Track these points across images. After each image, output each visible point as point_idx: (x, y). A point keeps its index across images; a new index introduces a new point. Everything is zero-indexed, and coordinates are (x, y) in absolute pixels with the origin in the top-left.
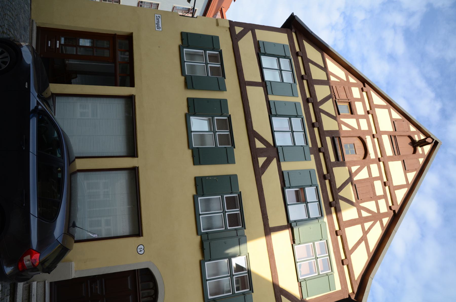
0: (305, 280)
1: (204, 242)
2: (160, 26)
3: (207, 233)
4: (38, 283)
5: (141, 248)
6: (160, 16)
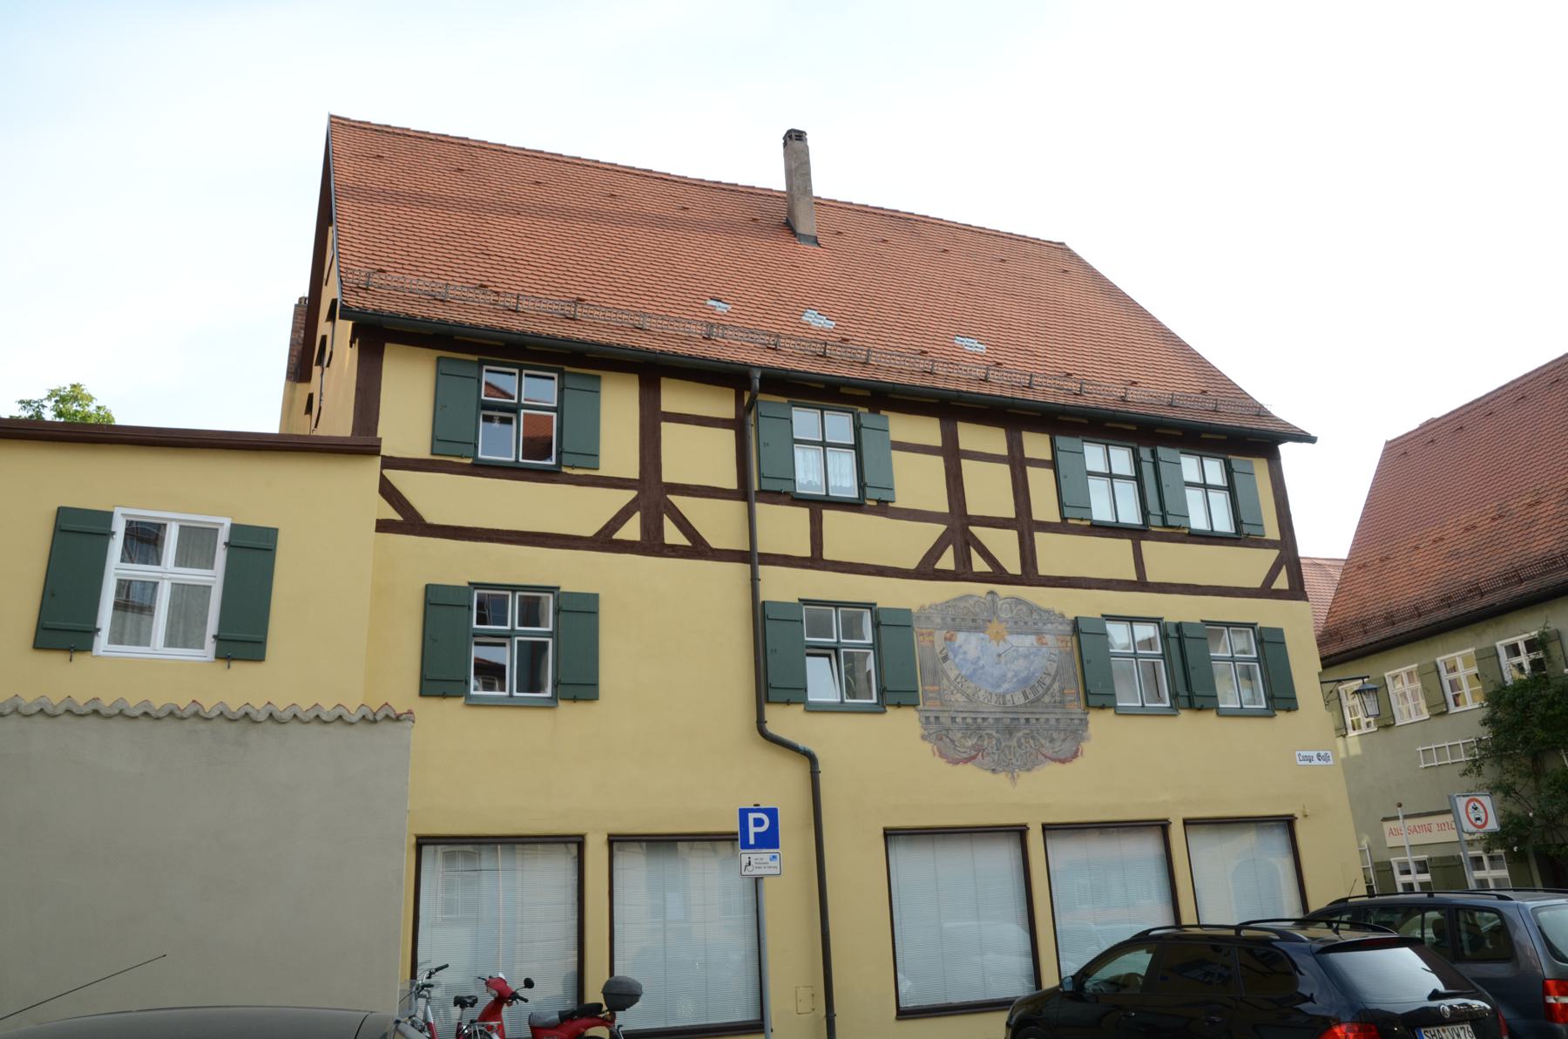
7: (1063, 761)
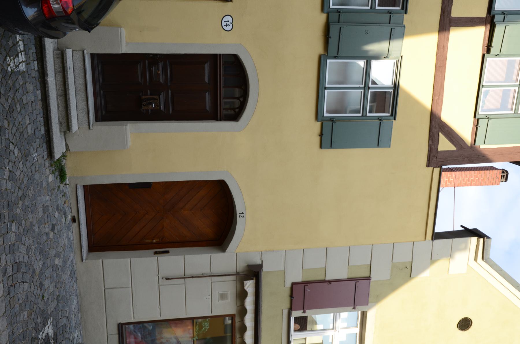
0: (488, 118)
1: (331, 26)
3: (338, 11)
4: (74, 52)
5: (229, 22)
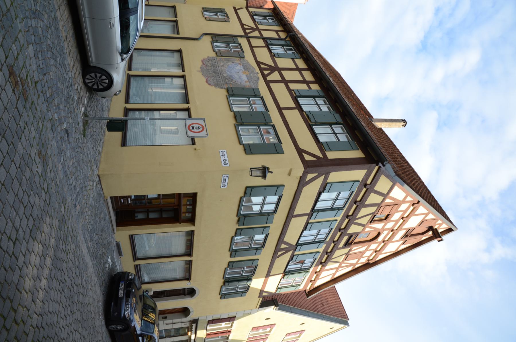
2: (226, 184)
6: (228, 175)
7: (207, 81)
